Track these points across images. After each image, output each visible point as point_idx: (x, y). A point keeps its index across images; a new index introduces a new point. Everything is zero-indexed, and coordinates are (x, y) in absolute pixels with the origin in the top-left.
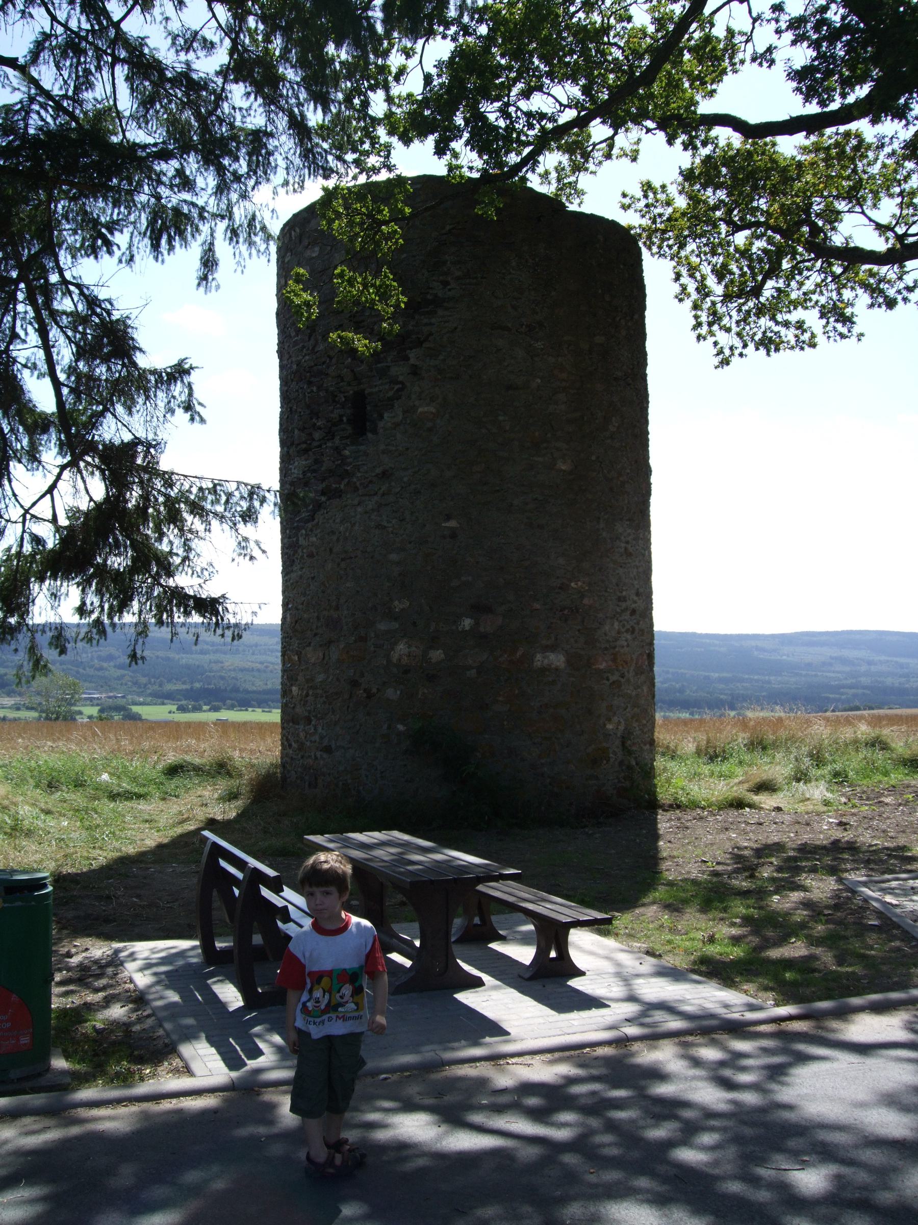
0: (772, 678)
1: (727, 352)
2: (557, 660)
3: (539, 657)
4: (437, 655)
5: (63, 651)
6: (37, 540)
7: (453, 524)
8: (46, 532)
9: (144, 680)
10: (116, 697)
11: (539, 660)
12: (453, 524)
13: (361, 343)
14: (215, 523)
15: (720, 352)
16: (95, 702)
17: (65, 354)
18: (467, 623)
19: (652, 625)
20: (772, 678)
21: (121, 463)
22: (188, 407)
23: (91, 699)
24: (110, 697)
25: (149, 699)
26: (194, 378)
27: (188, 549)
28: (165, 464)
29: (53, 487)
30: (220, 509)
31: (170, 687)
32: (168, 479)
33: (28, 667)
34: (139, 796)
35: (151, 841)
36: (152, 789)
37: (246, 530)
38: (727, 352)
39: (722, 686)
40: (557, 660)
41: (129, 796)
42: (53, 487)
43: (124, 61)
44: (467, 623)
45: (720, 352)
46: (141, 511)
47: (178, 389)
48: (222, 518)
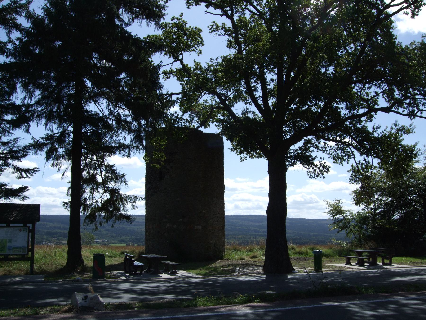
0: (332, 235)
1: (243, 158)
2: (200, 227)
3: (196, 227)
4: (175, 226)
5: (101, 225)
6: (98, 205)
7: (178, 199)
8: (100, 204)
9: (114, 235)
10: (105, 241)
11: (196, 227)
12: (178, 199)
13: (158, 166)
14: (129, 203)
15: (242, 158)
16: (98, 243)
17: (104, 173)
18: (181, 220)
19: (286, 215)
20: (332, 235)
21: (113, 192)
22: (125, 182)
23: (97, 242)
24: (103, 241)
25: (116, 242)
26: (126, 177)
27: (124, 207)
28: (120, 192)
29: (101, 196)
30: (130, 200)
31: (124, 238)
32: (121, 195)
33: (95, 228)
34: (115, 257)
35: (117, 263)
36: (117, 256)
37: (134, 204)
38: (243, 158)
39: (314, 238)
40: (200, 227)
41: (112, 257)
42: (101, 196)
43: (114, 120)
44: (181, 220)
45: (242, 158)
46: (116, 200)
47: (123, 179)
48: (130, 202)
